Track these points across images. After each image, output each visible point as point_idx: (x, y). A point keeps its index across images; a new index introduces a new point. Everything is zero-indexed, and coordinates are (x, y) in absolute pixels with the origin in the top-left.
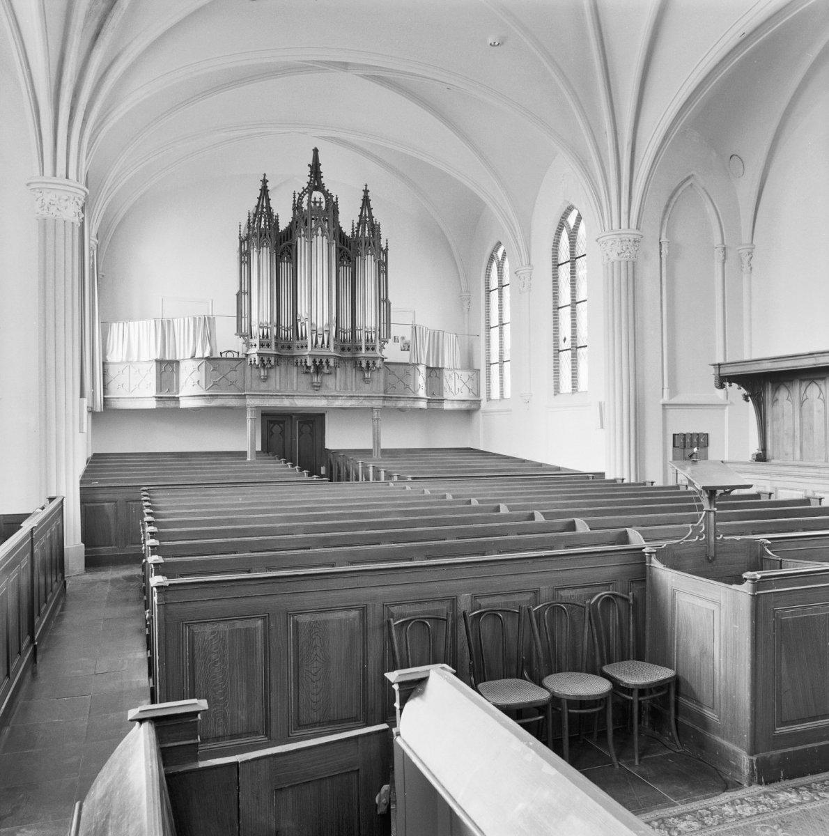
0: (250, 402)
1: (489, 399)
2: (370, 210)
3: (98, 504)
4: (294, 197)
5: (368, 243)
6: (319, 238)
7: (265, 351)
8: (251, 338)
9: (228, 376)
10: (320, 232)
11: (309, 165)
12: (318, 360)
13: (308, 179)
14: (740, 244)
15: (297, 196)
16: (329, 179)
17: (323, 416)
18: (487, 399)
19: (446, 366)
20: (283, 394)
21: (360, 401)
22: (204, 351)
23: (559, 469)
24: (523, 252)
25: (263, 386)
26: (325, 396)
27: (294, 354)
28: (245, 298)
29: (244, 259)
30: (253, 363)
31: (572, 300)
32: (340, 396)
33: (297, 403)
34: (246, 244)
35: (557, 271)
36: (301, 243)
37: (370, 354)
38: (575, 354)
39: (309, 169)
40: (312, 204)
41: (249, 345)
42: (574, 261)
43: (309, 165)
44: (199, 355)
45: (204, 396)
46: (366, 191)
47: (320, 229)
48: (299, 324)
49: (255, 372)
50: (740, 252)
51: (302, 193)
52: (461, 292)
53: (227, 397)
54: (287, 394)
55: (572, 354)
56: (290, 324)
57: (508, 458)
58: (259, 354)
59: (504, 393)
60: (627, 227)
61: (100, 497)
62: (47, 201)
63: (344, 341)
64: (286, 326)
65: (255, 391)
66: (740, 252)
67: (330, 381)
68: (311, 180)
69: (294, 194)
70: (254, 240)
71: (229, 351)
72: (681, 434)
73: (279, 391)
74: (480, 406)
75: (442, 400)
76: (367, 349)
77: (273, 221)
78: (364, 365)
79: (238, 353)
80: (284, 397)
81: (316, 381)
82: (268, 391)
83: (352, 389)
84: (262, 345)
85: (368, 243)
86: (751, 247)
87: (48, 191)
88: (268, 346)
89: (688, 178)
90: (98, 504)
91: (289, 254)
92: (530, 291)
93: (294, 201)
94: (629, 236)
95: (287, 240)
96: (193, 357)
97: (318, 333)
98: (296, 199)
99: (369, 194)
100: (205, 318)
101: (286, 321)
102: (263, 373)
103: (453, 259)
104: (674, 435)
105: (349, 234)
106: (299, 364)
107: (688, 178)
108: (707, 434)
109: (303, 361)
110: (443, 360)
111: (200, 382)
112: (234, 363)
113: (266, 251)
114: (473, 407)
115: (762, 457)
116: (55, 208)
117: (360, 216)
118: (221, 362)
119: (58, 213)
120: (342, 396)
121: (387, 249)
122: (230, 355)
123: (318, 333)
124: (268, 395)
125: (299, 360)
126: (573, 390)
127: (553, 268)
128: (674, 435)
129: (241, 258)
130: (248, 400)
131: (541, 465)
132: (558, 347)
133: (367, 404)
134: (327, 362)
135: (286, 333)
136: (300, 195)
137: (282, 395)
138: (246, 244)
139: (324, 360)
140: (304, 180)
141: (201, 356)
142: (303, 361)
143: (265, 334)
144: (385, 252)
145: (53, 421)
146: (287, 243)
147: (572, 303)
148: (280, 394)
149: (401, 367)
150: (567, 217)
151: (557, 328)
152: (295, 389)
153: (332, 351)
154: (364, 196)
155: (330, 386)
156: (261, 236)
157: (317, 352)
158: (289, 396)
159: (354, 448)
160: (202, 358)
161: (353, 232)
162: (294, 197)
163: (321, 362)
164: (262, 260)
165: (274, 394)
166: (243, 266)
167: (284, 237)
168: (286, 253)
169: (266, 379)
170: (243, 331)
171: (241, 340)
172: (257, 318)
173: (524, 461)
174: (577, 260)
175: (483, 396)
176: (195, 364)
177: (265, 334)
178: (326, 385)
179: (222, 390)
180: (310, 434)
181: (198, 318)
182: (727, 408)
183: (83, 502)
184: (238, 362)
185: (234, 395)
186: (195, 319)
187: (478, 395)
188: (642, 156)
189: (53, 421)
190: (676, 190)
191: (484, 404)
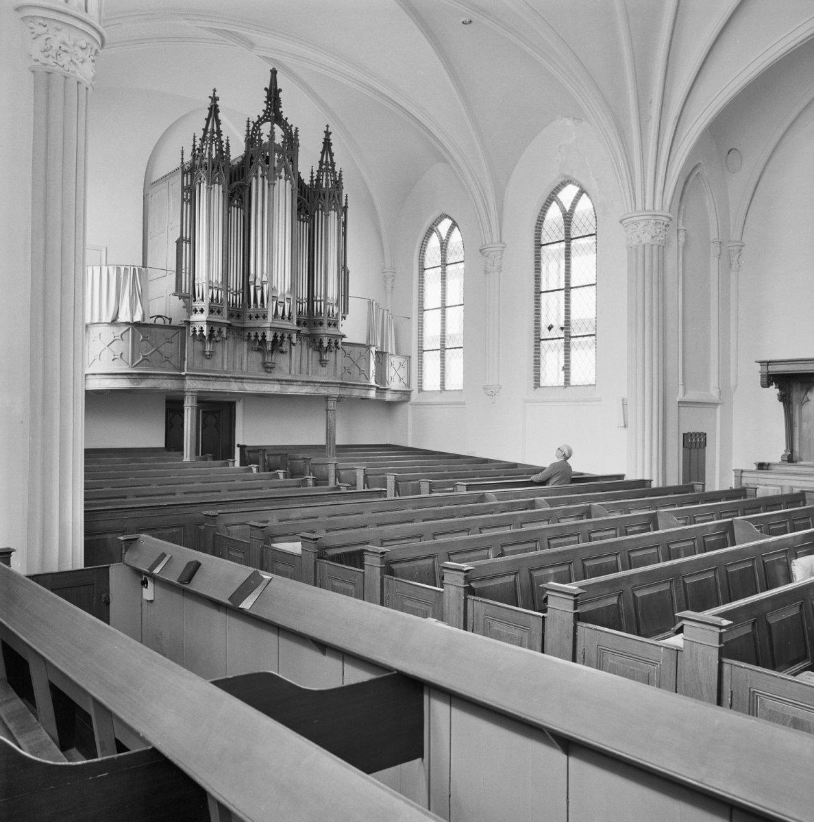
0: (190, 385)
1: (421, 390)
2: (332, 155)
3: (97, 537)
4: (248, 126)
5: (332, 196)
6: (282, 181)
7: (216, 318)
8: (195, 301)
9: (162, 349)
10: (283, 174)
11: (266, 89)
12: (279, 334)
13: (264, 106)
14: (730, 241)
15: (251, 125)
16: (286, 111)
17: (232, 405)
18: (419, 389)
19: (389, 351)
20: (232, 375)
21: (316, 388)
22: (133, 313)
23: (582, 474)
24: (494, 223)
25: (207, 363)
26: (278, 380)
27: (246, 325)
28: (186, 247)
29: (187, 196)
30: (198, 333)
31: (566, 284)
32: (294, 381)
33: (246, 387)
34: (189, 176)
35: (540, 252)
36: (257, 185)
37: (331, 330)
38: (569, 343)
39: (265, 93)
40: (197, 152)
41: (191, 310)
42: (569, 242)
43: (266, 89)
44: (124, 317)
45: (131, 374)
46: (328, 133)
47: (283, 170)
48: (252, 287)
49: (199, 345)
50: (731, 248)
51: (257, 122)
52: (385, 268)
53: (161, 377)
54: (236, 376)
55: (565, 343)
56: (240, 287)
57: (458, 457)
58: (208, 322)
59: (446, 384)
60: (652, 208)
61: (102, 525)
62: (55, 44)
63: (283, 317)
64: (235, 289)
65: (197, 371)
66: (731, 248)
67: (282, 361)
68: (268, 108)
69: (248, 121)
70: (202, 173)
71: (160, 316)
72: (689, 433)
73: (227, 372)
74: (410, 398)
75: (385, 389)
76: (329, 325)
77: (223, 154)
78: (325, 344)
79: (170, 319)
80: (232, 380)
81: (270, 361)
82: (214, 371)
83: (308, 374)
84: (211, 311)
85: (332, 196)
86: (740, 244)
87: (59, 26)
88: (219, 312)
89: (696, 167)
90: (97, 537)
91: (241, 197)
92: (501, 271)
93: (248, 131)
94: (663, 218)
95: (239, 180)
96: (114, 322)
97: (279, 300)
98: (251, 129)
99: (331, 137)
100: (134, 269)
101: (235, 282)
102: (208, 347)
103: (379, 233)
104: (684, 434)
105: (307, 182)
106: (253, 338)
107: (696, 167)
108: (705, 434)
109: (260, 335)
110: (387, 345)
111: (123, 356)
112: (170, 332)
113: (218, 189)
114: (404, 398)
115: (790, 459)
116: (69, 59)
117: (321, 162)
118: (153, 330)
119: (73, 68)
120: (297, 381)
121: (346, 207)
122: (160, 321)
123: (279, 300)
124: (213, 376)
125: (253, 334)
126: (565, 383)
127: (536, 248)
128: (684, 434)
129: (183, 195)
130: (188, 382)
131: (515, 465)
132: (539, 335)
133: (323, 391)
134: (290, 338)
135: (234, 297)
136: (255, 124)
137: (231, 377)
138: (189, 176)
139: (286, 335)
140: (258, 107)
141: (129, 320)
142: (260, 335)
143: (215, 297)
144: (345, 209)
145: (57, 405)
146: (235, 183)
147: (566, 288)
148: (228, 375)
149: (356, 348)
150: (558, 192)
151: (539, 314)
152: (245, 369)
153: (292, 325)
154: (325, 139)
155: (284, 368)
156: (213, 168)
157: (281, 324)
158: (238, 378)
159: (123, 446)
160: (128, 323)
161: (312, 181)
162: (248, 126)
163: (282, 337)
164: (210, 199)
165: (222, 375)
166: (185, 205)
167: (239, 171)
168: (237, 196)
169: (210, 356)
170: (183, 292)
171: (181, 302)
172: (204, 274)
173: (486, 461)
174: (573, 241)
175: (414, 386)
176: (108, 333)
177: (215, 297)
178: (280, 368)
179: (154, 368)
180: (215, 426)
181: (122, 269)
182: (719, 407)
183: (88, 532)
184: (175, 332)
185: (168, 375)
186: (118, 269)
187: (408, 385)
188: (684, 134)
189: (57, 405)
190: (689, 177)
191: (414, 396)
